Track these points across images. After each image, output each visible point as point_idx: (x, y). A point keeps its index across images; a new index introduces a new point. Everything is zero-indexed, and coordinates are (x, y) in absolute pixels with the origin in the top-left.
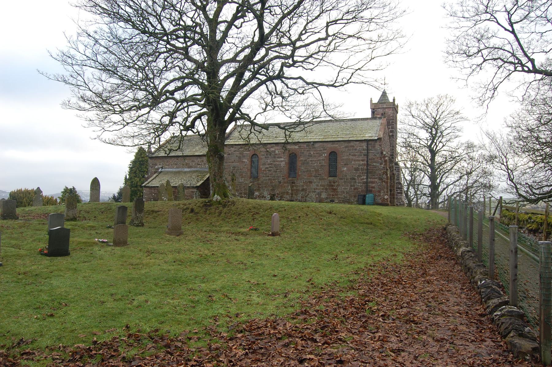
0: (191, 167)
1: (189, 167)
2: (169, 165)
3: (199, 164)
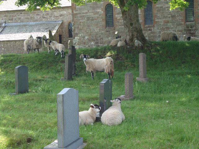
0: (37, 21)
1: (34, 21)
2: (12, 20)
3: (45, 18)
